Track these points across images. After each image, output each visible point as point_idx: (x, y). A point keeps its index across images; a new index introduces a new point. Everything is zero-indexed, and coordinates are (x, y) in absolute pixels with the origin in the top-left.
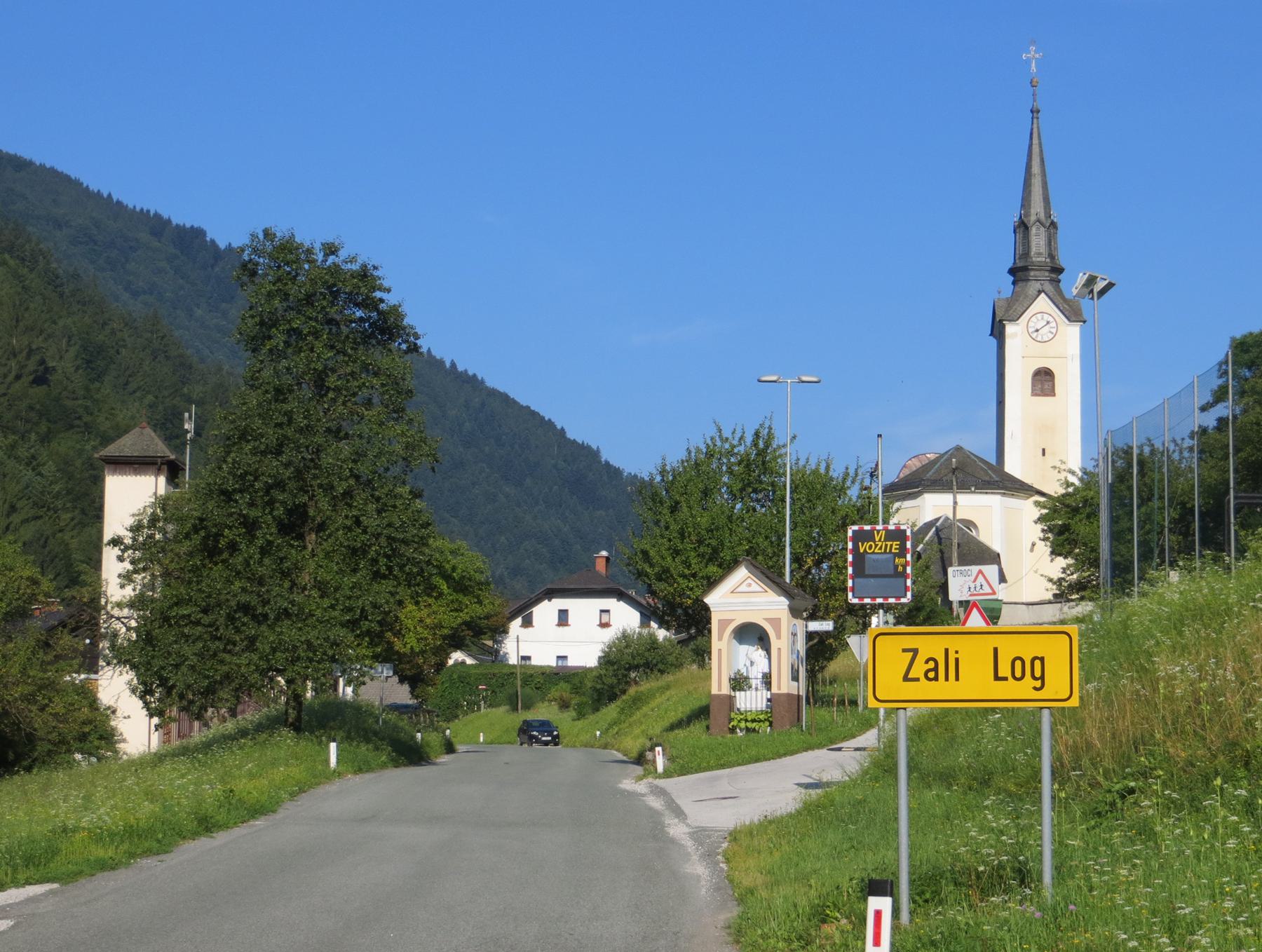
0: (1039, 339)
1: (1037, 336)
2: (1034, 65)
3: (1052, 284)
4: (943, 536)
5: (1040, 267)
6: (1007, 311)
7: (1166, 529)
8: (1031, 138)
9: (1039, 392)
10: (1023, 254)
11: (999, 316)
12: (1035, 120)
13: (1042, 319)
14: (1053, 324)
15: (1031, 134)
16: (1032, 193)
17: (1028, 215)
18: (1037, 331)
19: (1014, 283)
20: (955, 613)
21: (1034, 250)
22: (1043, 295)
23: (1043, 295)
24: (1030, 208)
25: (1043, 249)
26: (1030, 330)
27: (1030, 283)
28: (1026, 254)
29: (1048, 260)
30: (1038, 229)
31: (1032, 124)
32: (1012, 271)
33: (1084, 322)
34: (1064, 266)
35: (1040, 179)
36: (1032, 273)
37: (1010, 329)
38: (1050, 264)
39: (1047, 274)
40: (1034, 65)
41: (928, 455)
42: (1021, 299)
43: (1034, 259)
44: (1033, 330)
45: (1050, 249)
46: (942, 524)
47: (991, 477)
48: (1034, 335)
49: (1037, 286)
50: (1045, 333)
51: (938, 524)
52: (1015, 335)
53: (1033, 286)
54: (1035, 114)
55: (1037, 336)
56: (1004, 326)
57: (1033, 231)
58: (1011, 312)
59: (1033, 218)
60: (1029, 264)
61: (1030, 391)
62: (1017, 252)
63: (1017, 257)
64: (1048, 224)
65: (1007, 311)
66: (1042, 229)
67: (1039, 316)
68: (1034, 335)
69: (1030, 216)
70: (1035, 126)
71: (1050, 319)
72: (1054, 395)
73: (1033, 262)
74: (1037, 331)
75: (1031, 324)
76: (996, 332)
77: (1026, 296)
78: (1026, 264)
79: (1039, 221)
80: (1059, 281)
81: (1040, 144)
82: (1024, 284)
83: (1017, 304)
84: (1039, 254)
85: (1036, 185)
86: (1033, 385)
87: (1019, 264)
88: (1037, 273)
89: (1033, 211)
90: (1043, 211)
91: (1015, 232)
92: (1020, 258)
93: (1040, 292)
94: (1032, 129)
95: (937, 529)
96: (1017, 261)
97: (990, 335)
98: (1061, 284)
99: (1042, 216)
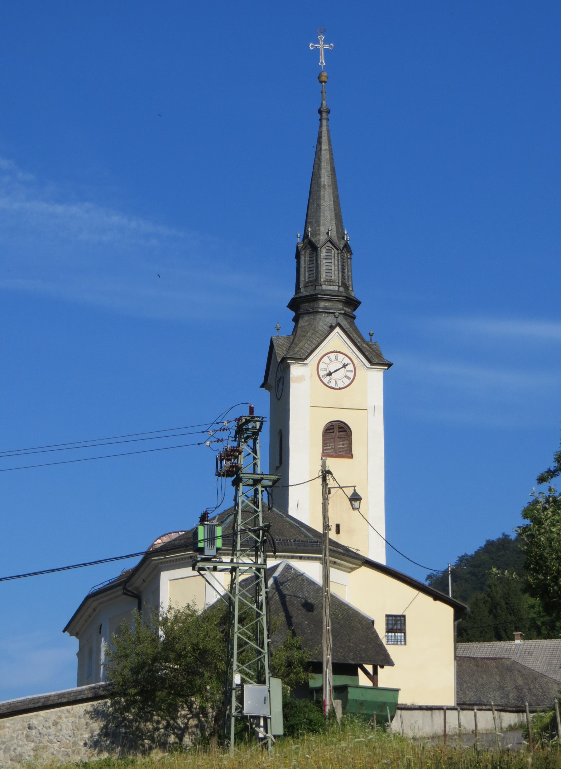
0: (332, 384)
1: (330, 381)
2: (322, 57)
3: (346, 319)
4: (286, 592)
5: (332, 297)
6: (292, 344)
7: (233, 720)
8: (319, 143)
9: (331, 452)
10: (308, 282)
11: (280, 353)
12: (324, 122)
13: (337, 360)
14: (350, 367)
15: (320, 138)
16: (322, 207)
17: (316, 233)
18: (330, 374)
19: (296, 320)
20: (328, 708)
21: (323, 276)
22: (338, 329)
23: (338, 329)
24: (319, 225)
25: (335, 275)
26: (322, 373)
27: (319, 316)
28: (315, 281)
29: (342, 289)
30: (329, 251)
31: (321, 125)
32: (294, 305)
33: (389, 365)
34: (359, 299)
35: (331, 191)
36: (322, 304)
37: (296, 370)
38: (345, 294)
39: (340, 306)
40: (322, 57)
41: (180, 533)
42: (309, 334)
43: (324, 287)
44: (325, 373)
45: (343, 276)
46: (282, 574)
47: (306, 536)
48: (347, 361)
49: (330, 320)
50: (339, 379)
51: (276, 574)
52: (301, 379)
53: (324, 321)
54: (324, 115)
55: (330, 381)
56: (288, 367)
57: (323, 253)
58: (297, 349)
59: (323, 238)
60: (317, 292)
61: (321, 450)
62: (302, 279)
63: (302, 285)
64: (342, 246)
65: (292, 344)
66: (334, 252)
67: (332, 356)
68: (326, 380)
69: (319, 234)
70: (324, 129)
71: (347, 361)
72: (352, 457)
73: (322, 290)
74: (330, 374)
75: (322, 366)
76: (271, 381)
77: (315, 332)
78: (315, 292)
79: (330, 241)
80: (354, 318)
81: (331, 152)
82: (312, 317)
83: (304, 341)
84: (330, 282)
85: (327, 198)
86: (325, 444)
87: (304, 292)
88: (328, 304)
89: (323, 229)
90: (334, 228)
91: (298, 256)
92: (305, 287)
93: (332, 328)
94: (320, 133)
95: (276, 580)
96: (302, 290)
97: (262, 386)
98: (355, 321)
99: (334, 234)
